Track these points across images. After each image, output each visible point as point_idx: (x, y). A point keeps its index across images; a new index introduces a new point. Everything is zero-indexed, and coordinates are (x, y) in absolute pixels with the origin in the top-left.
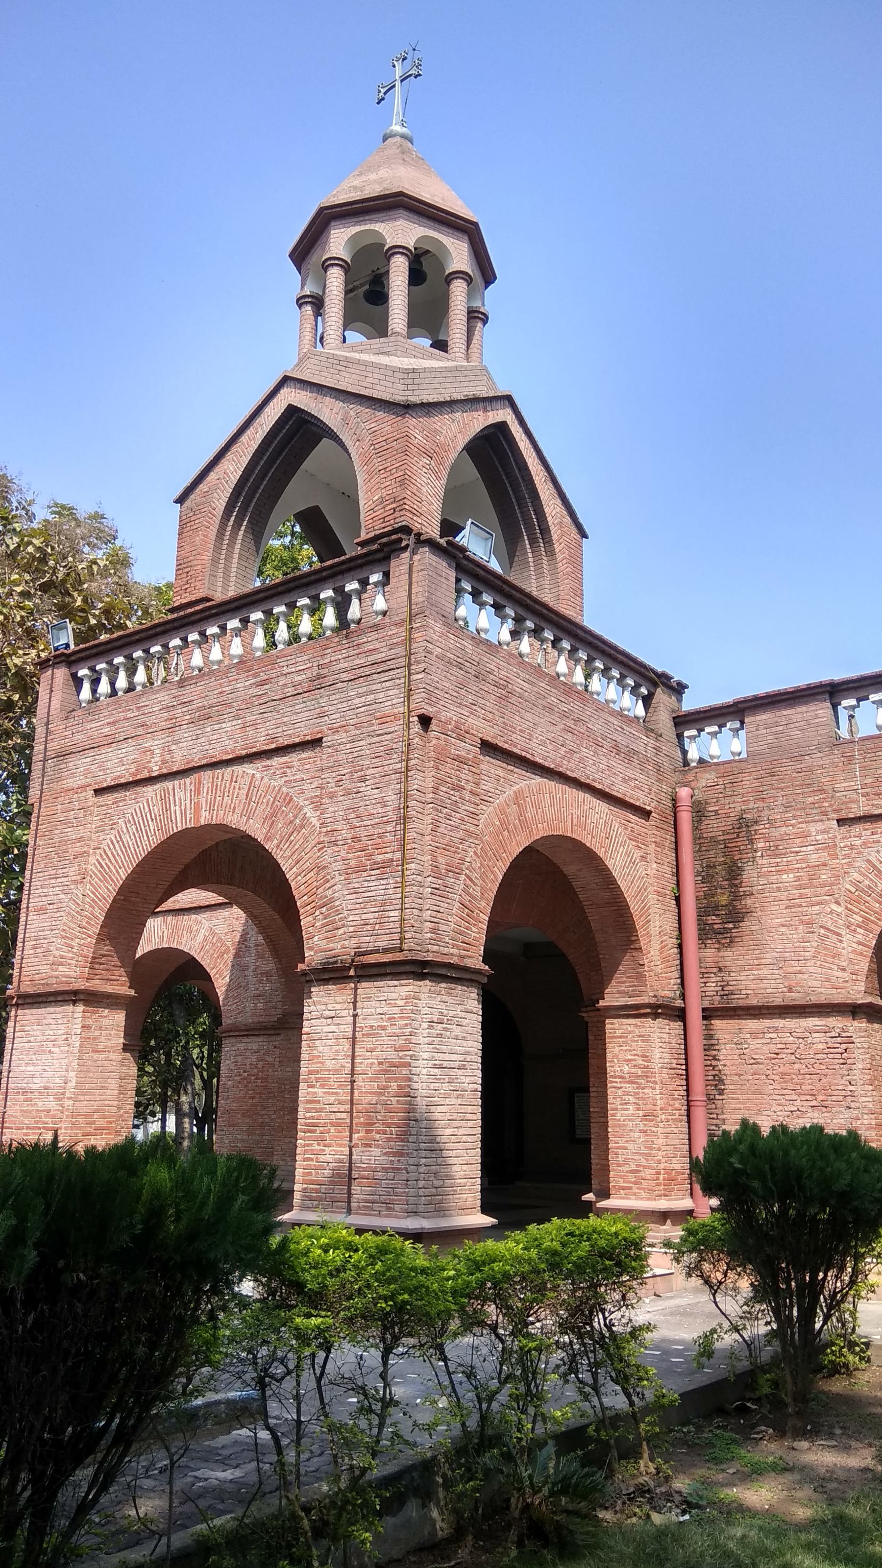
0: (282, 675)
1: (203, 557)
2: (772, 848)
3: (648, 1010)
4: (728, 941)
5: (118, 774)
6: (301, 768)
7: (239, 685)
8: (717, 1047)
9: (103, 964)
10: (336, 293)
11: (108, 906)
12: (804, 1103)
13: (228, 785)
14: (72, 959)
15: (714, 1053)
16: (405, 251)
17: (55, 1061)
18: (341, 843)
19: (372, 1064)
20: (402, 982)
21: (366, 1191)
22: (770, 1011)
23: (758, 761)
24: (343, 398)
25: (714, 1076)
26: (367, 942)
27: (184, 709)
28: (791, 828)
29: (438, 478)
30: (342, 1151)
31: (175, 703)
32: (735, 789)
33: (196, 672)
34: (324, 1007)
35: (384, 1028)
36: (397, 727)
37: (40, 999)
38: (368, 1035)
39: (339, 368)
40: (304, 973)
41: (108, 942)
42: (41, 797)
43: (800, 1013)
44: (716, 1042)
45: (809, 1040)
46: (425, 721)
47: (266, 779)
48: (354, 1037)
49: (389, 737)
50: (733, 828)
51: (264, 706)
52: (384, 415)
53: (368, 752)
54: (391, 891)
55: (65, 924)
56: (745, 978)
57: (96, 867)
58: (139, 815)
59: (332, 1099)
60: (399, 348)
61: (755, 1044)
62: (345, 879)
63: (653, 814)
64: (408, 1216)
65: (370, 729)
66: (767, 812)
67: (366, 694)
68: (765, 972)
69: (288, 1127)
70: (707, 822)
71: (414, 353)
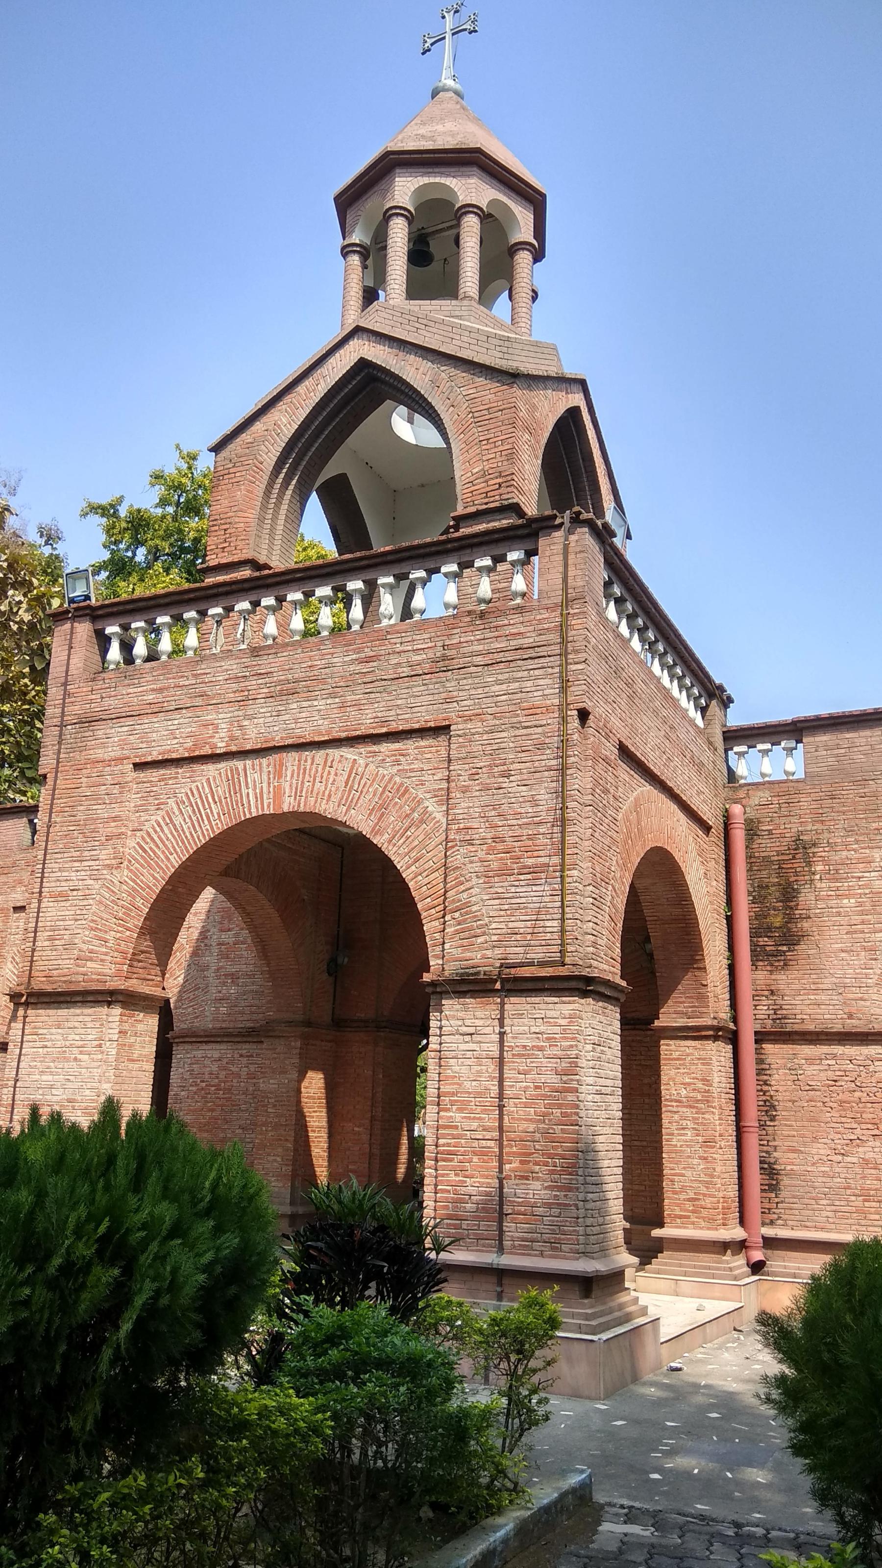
0: (394, 653)
1: (246, 515)
2: (832, 872)
3: (711, 1033)
4: (782, 963)
5: (168, 747)
6: (419, 756)
7: (335, 660)
8: (768, 1072)
9: (141, 962)
10: (400, 244)
11: (154, 897)
12: (865, 1132)
13: (320, 769)
14: (106, 954)
15: (765, 1078)
16: (479, 212)
17: (84, 1070)
18: (478, 842)
19: (526, 1087)
20: (564, 999)
21: (523, 1228)
22: (829, 1037)
23: (817, 782)
24: (432, 358)
25: (765, 1101)
26: (516, 954)
27: (260, 681)
28: (853, 853)
29: (537, 457)
30: (488, 1183)
31: (248, 674)
32: (791, 809)
33: (270, 642)
34: (460, 1023)
35: (541, 1049)
36: (552, 720)
37: (62, 999)
38: (520, 1056)
39: (417, 325)
40: (433, 984)
41: (148, 937)
42: (57, 767)
43: (862, 1041)
44: (767, 1067)
45: (871, 1068)
46: (584, 715)
47: (372, 767)
48: (501, 1058)
49: (540, 730)
50: (789, 849)
51: (369, 686)
52: (486, 382)
53: (511, 745)
54: (547, 899)
55: (94, 914)
56: (800, 1002)
57: (137, 851)
58: (197, 796)
59: (475, 1125)
60: (473, 314)
61: (811, 1070)
62: (485, 883)
63: (713, 830)
64: (580, 1257)
65: (515, 720)
66: (826, 835)
67: (509, 681)
68: (823, 997)
69: (271, 1145)
70: (760, 841)
71: (486, 321)
